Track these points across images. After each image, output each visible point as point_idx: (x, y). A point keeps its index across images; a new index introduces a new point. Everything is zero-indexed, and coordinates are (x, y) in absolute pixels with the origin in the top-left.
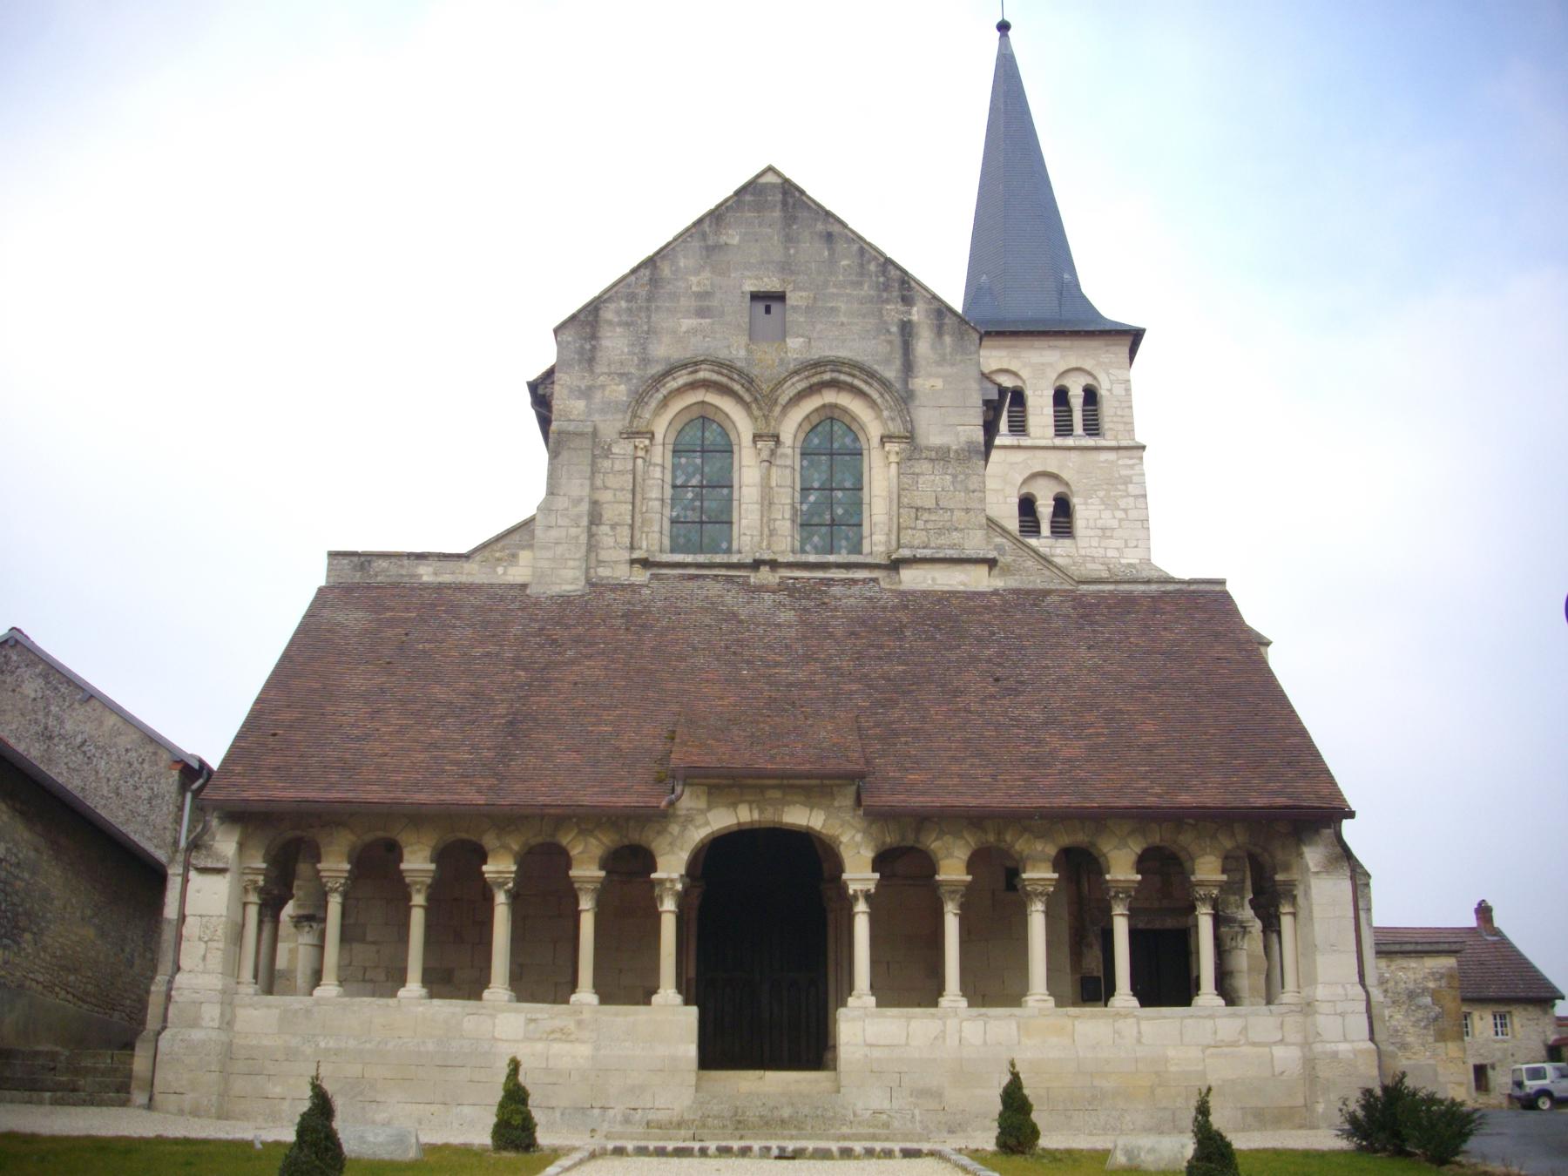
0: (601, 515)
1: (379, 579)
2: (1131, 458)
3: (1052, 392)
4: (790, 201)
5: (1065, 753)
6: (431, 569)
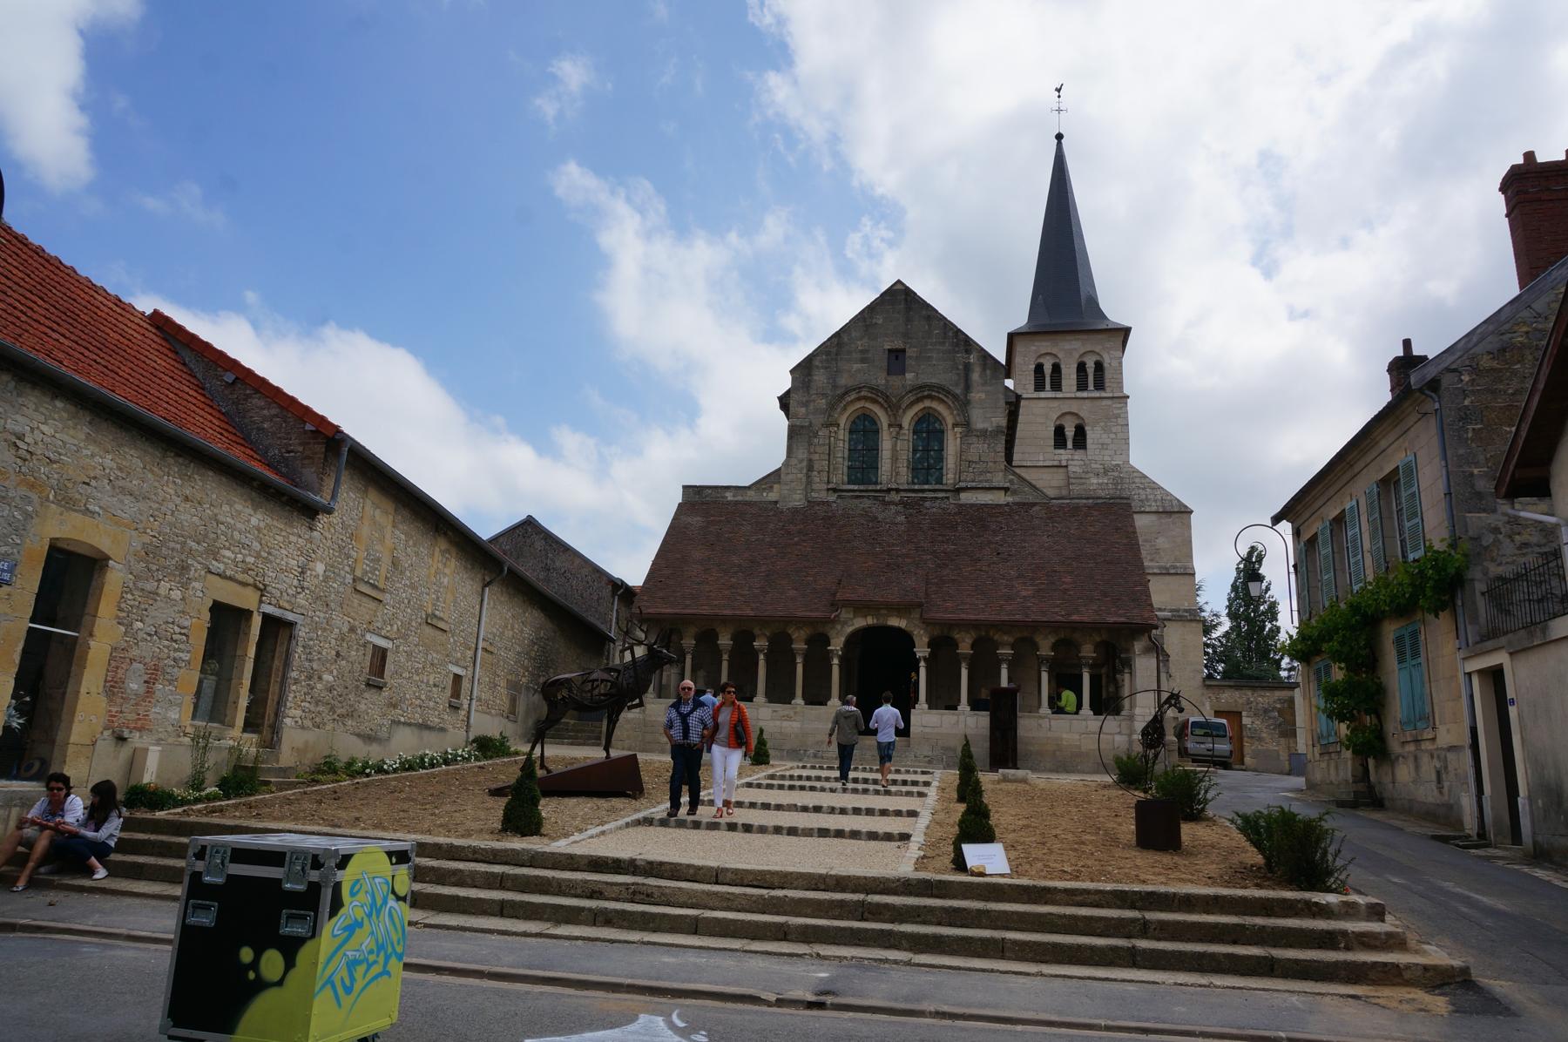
1: (707, 499)
2: (1120, 403)
5: (1024, 593)
6: (731, 494)
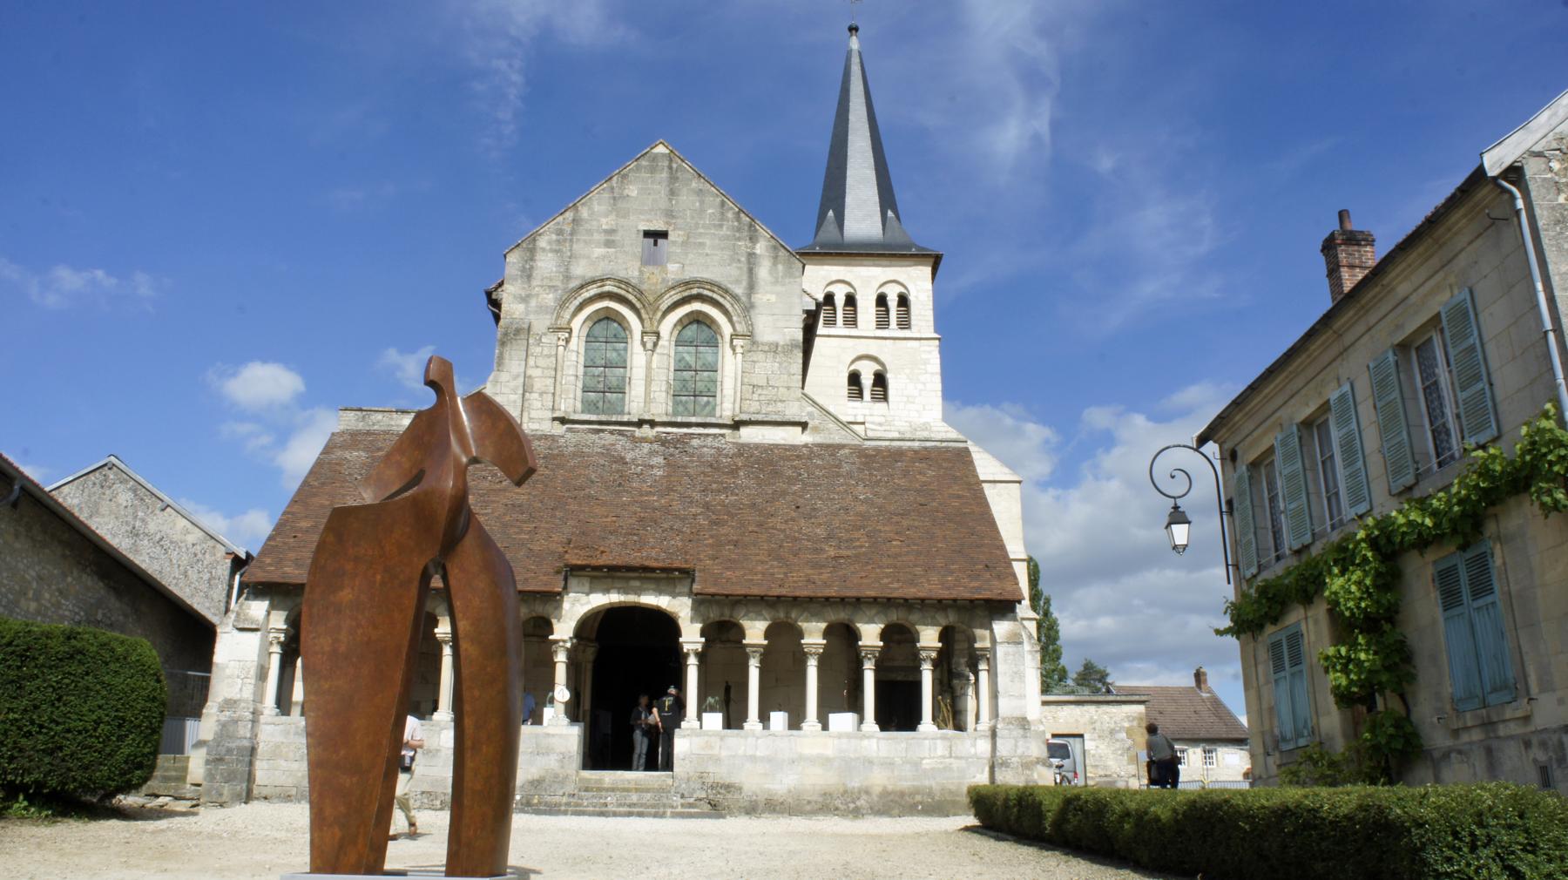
0: (532, 385)
1: (375, 427)
3: (875, 297)
4: (674, 166)
